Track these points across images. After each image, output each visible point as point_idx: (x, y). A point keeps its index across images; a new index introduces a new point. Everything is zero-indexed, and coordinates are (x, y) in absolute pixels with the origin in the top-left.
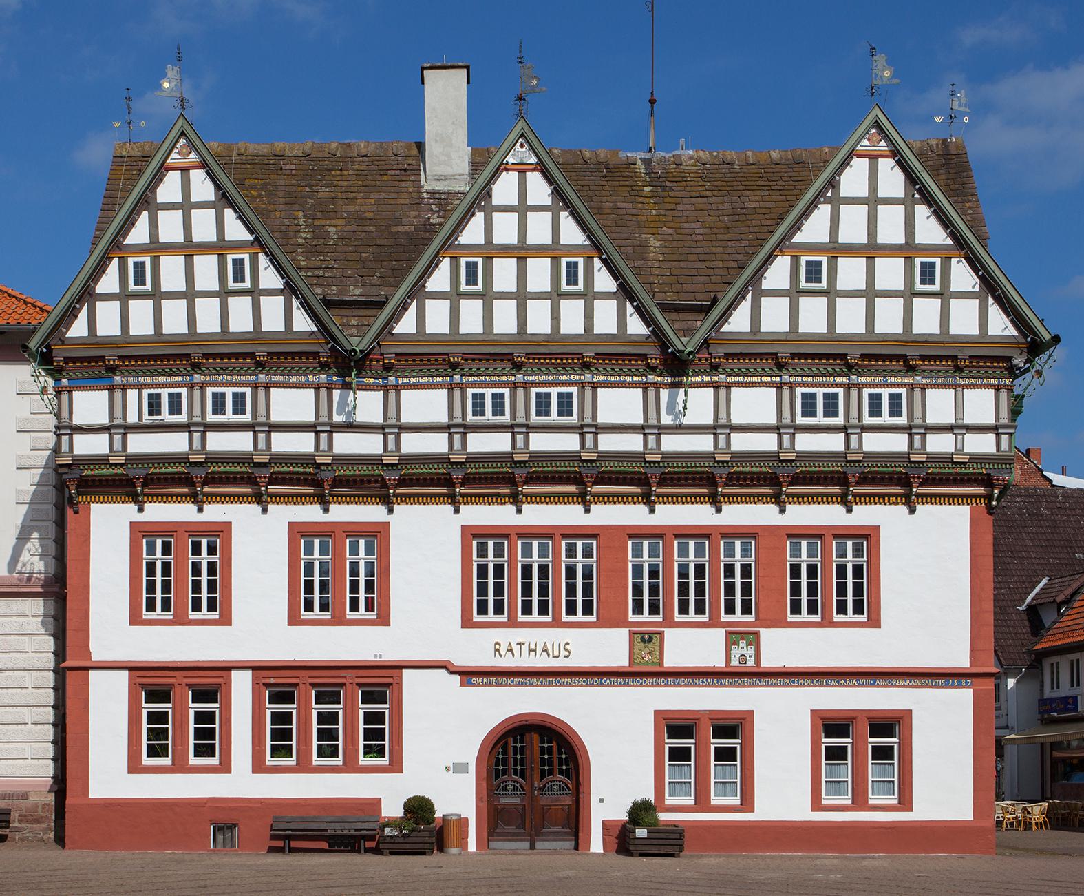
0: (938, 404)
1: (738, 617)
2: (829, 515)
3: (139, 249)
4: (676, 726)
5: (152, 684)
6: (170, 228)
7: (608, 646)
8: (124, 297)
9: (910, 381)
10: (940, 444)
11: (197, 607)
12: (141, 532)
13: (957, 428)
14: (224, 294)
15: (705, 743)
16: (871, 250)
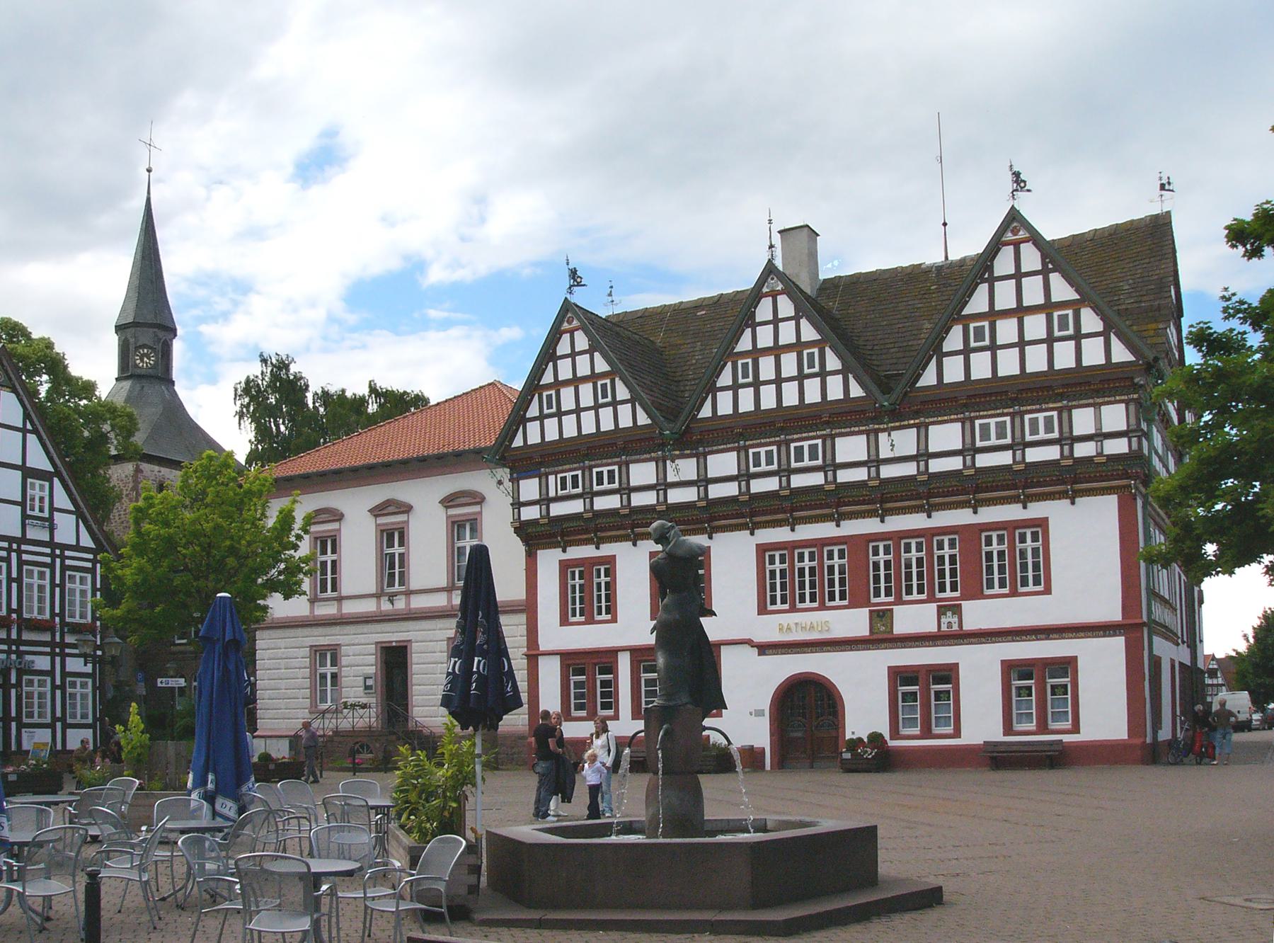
0: (1083, 421)
1: (948, 594)
2: (1012, 512)
3: (548, 387)
4: (899, 676)
5: (573, 661)
6: (765, 337)
7: (855, 622)
8: (541, 418)
9: (1059, 405)
10: (1084, 450)
11: (574, 615)
12: (565, 566)
13: (1099, 436)
14: (597, 407)
15: (925, 689)
16: (576, 381)
